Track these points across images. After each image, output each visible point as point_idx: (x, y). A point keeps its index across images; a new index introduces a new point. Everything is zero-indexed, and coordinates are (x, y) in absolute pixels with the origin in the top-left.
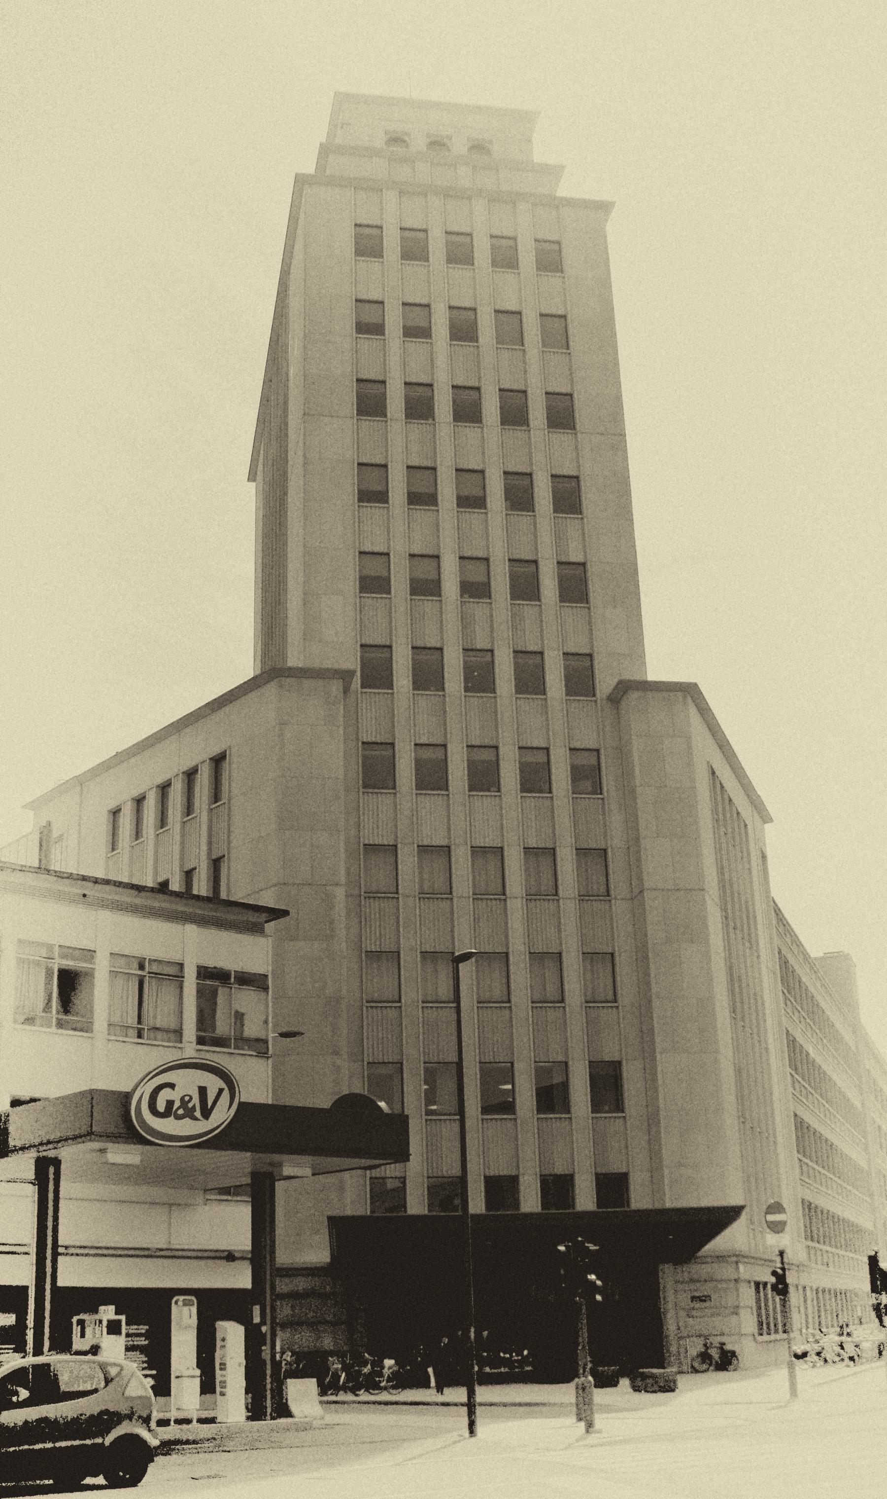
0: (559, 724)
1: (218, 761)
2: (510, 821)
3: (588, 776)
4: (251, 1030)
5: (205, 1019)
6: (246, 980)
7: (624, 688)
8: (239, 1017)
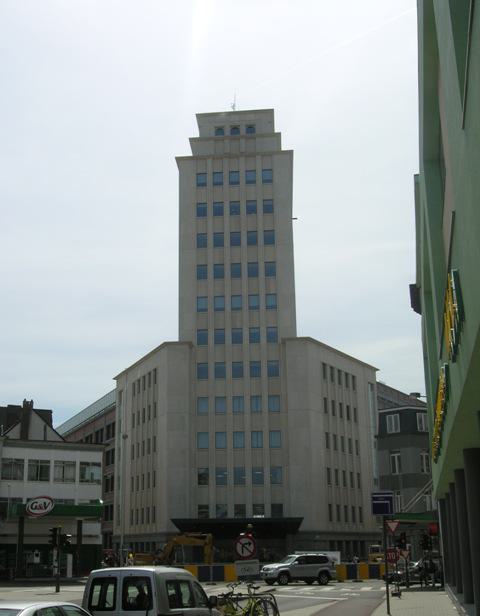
0: (263, 353)
1: (155, 370)
2: (246, 386)
3: (273, 372)
4: (96, 478)
5: (82, 476)
6: (95, 464)
7: (284, 341)
8: (92, 474)
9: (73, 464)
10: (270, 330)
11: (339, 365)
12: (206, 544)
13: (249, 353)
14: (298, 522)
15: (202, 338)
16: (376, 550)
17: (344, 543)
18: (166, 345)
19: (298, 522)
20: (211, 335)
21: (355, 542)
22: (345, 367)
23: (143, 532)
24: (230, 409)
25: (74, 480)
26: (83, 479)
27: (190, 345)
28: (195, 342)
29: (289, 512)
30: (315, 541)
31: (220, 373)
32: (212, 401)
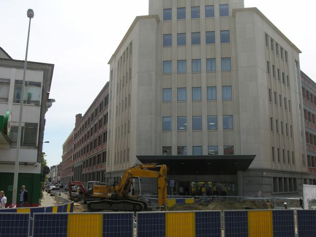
0: (217, 24)
2: (202, 51)
3: (225, 38)
8: (30, 95)
9: (7, 83)
10: (222, 7)
11: (277, 39)
12: (160, 176)
13: (204, 25)
14: (249, 159)
15: (167, 16)
16: (231, 187)
17: (293, 179)
18: (138, 19)
19: (249, 159)
20: (174, 13)
21: (290, 179)
22: (282, 43)
23: (121, 169)
24: (189, 69)
25: (7, 99)
26: (17, 99)
27: (156, 17)
28: (161, 17)
29: (240, 151)
30: (263, 177)
31: (182, 41)
32: (174, 64)
